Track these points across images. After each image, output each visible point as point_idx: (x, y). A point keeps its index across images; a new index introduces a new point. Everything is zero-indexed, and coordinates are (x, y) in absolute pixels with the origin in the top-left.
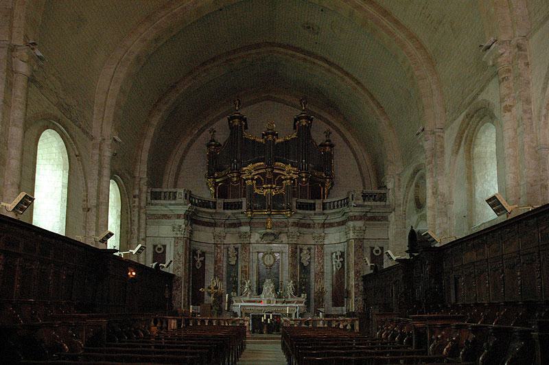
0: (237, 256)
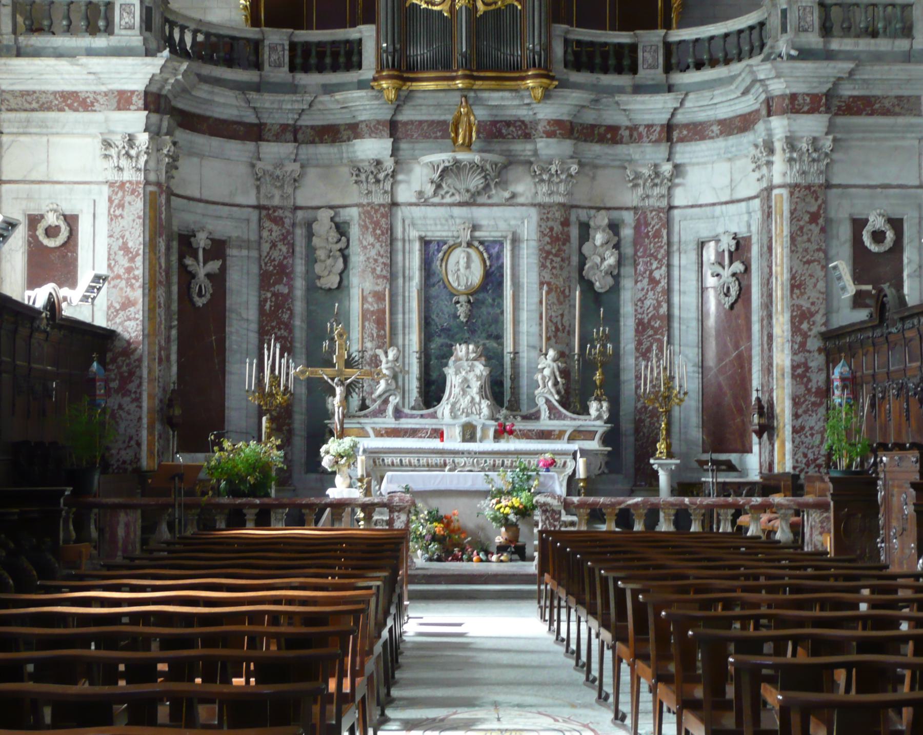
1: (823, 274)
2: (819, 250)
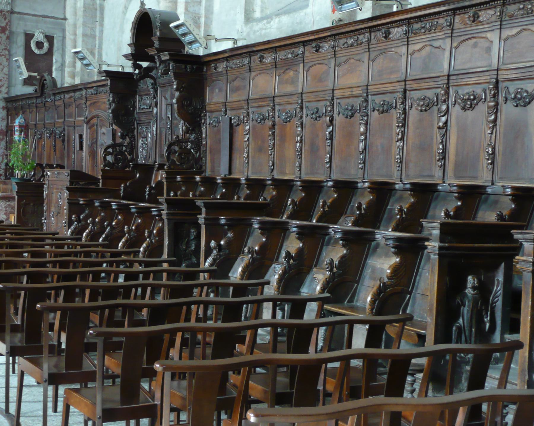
1: (7, 63)
2: (5, 49)
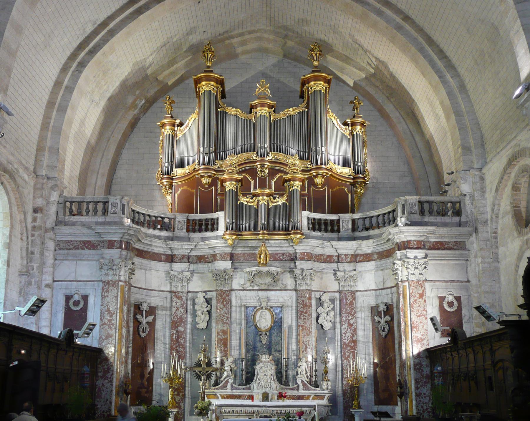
0: (209, 312)
2: (424, 310)
